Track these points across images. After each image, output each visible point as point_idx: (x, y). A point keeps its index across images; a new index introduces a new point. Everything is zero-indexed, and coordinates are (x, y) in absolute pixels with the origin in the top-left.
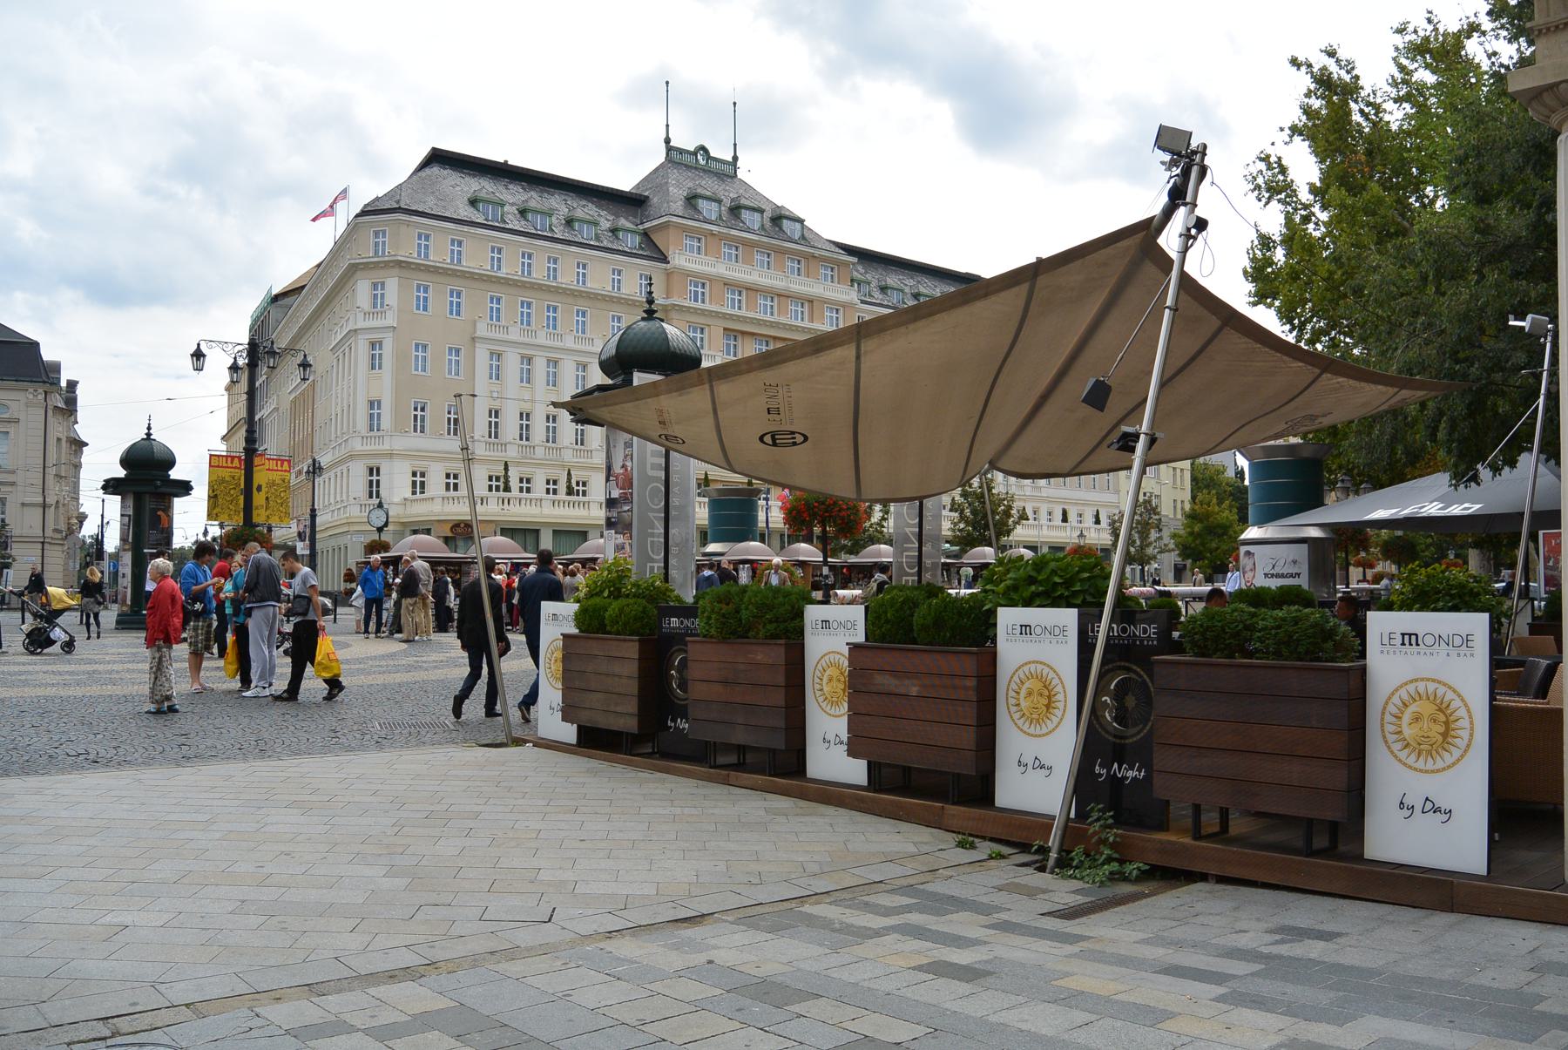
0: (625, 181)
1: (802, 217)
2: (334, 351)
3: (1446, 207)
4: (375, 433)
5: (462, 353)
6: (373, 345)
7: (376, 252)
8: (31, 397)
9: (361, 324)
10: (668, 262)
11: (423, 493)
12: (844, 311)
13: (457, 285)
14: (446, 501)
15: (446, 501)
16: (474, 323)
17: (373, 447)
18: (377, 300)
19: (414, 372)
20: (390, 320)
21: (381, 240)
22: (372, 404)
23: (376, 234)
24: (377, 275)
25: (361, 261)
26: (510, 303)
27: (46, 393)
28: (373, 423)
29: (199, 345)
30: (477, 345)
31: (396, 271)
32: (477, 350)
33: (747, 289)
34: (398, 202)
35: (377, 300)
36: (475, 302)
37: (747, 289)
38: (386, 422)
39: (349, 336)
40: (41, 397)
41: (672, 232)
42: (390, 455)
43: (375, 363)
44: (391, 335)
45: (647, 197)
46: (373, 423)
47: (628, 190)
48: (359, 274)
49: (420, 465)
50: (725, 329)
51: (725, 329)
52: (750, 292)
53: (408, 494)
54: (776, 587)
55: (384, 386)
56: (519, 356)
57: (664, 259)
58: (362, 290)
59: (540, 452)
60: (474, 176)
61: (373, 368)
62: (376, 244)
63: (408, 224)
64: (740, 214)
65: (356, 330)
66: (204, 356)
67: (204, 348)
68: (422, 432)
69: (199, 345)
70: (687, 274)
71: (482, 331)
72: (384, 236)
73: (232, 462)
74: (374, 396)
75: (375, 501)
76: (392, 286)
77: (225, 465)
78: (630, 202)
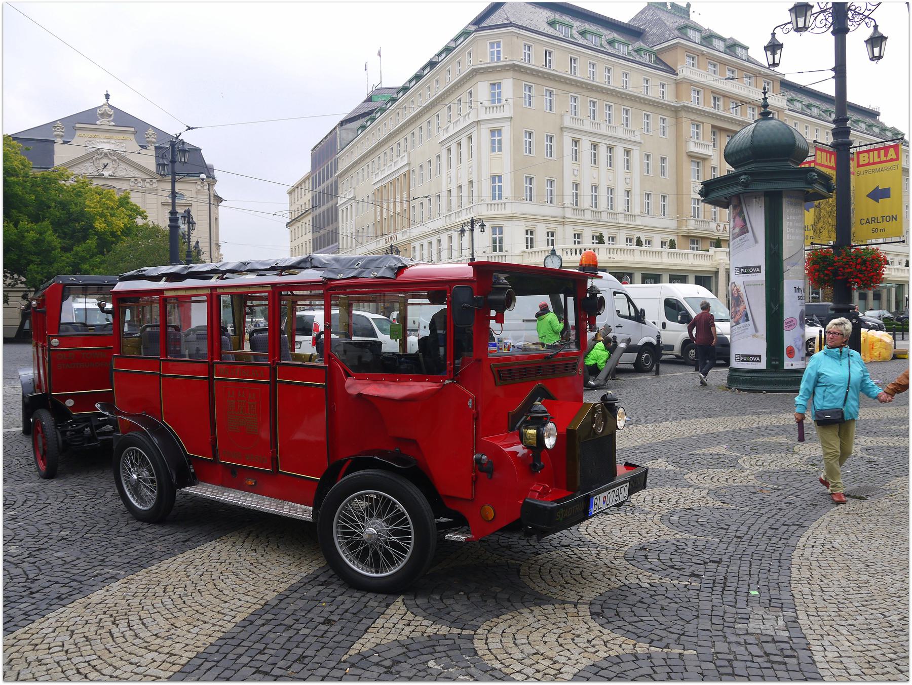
0: (624, 16)
1: (746, 44)
2: (443, 144)
3: (154, 230)
4: (497, 201)
5: (554, 139)
6: (493, 132)
7: (492, 59)
8: (199, 187)
9: (483, 116)
10: (677, 75)
11: (532, 247)
12: (778, 114)
13: (550, 85)
14: (530, 254)
15: (530, 254)
16: (562, 116)
17: (496, 212)
18: (496, 98)
19: (525, 154)
20: (507, 112)
21: (496, 49)
22: (493, 178)
23: (492, 45)
24: (494, 78)
25: (483, 66)
26: (584, 100)
27: (209, 184)
28: (497, 193)
29: (773, 34)
30: (565, 133)
31: (511, 74)
32: (564, 137)
33: (724, 96)
34: (508, 19)
35: (496, 98)
36: (563, 100)
37: (724, 96)
38: (507, 191)
39: (473, 125)
40: (206, 188)
41: (679, 51)
42: (511, 218)
43: (496, 146)
44: (508, 124)
45: (644, 30)
46: (497, 193)
47: (626, 22)
48: (478, 77)
49: (531, 225)
50: (713, 127)
51: (713, 127)
52: (725, 98)
53: (524, 248)
54: (487, 333)
55: (504, 163)
56: (590, 143)
57: (674, 72)
58: (482, 89)
59: (604, 216)
60: (541, 8)
61: (493, 150)
62: (492, 53)
63: (518, 36)
64: (712, 41)
65: (478, 122)
66: (781, 46)
67: (780, 38)
68: (531, 200)
69: (773, 34)
70: (691, 83)
71: (568, 122)
72: (498, 46)
73: (886, 155)
74: (496, 171)
75: (551, 248)
76: (508, 86)
77: (877, 160)
78: (631, 32)
